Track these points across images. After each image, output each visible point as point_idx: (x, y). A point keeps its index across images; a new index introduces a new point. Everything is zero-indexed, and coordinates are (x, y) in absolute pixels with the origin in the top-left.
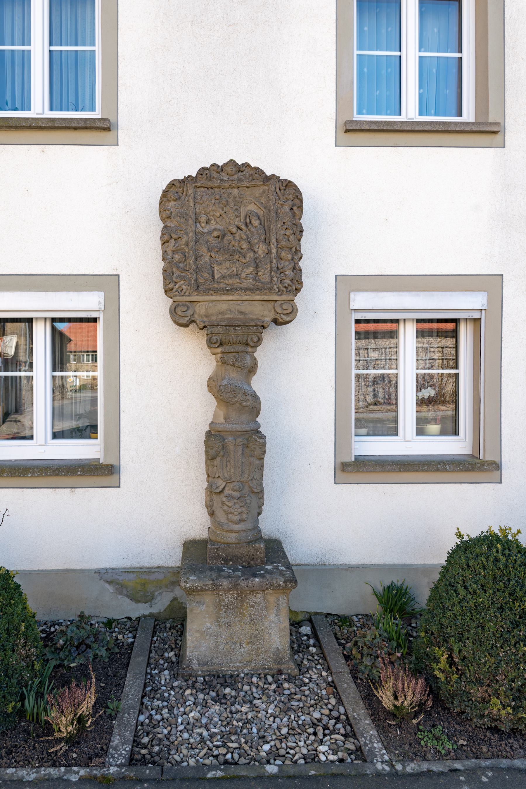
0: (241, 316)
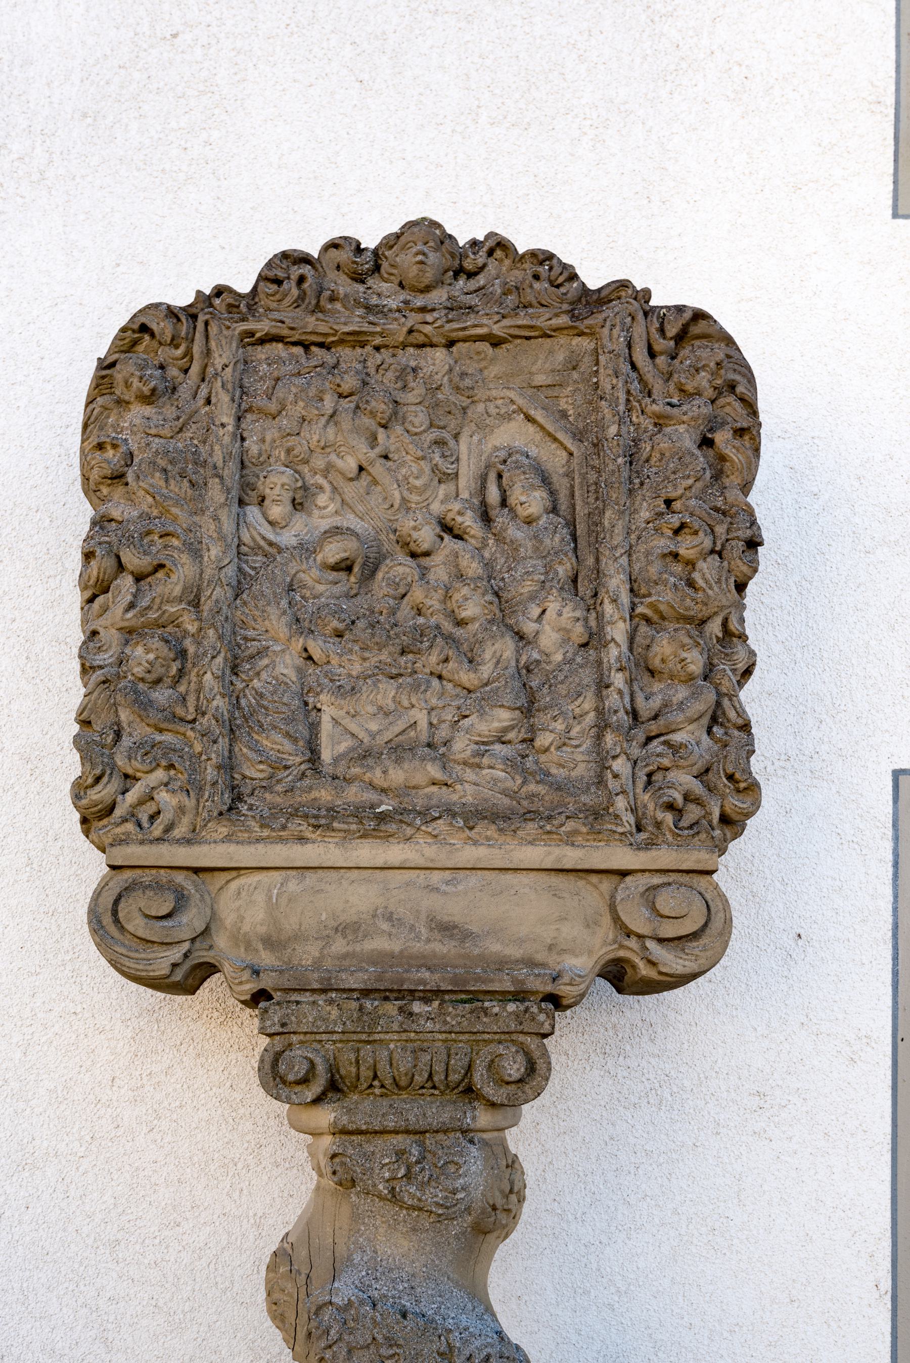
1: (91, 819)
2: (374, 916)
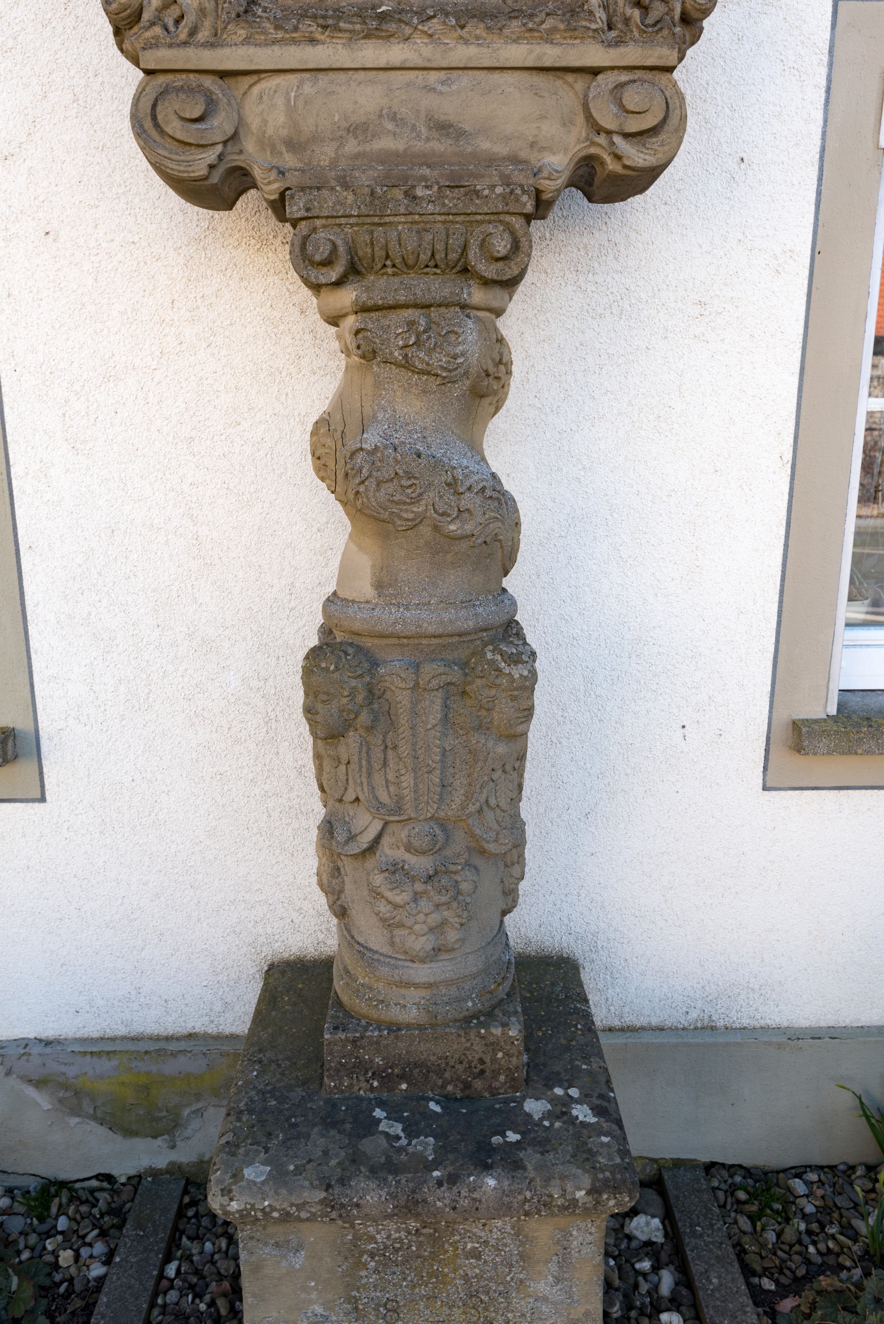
2: (380, 116)
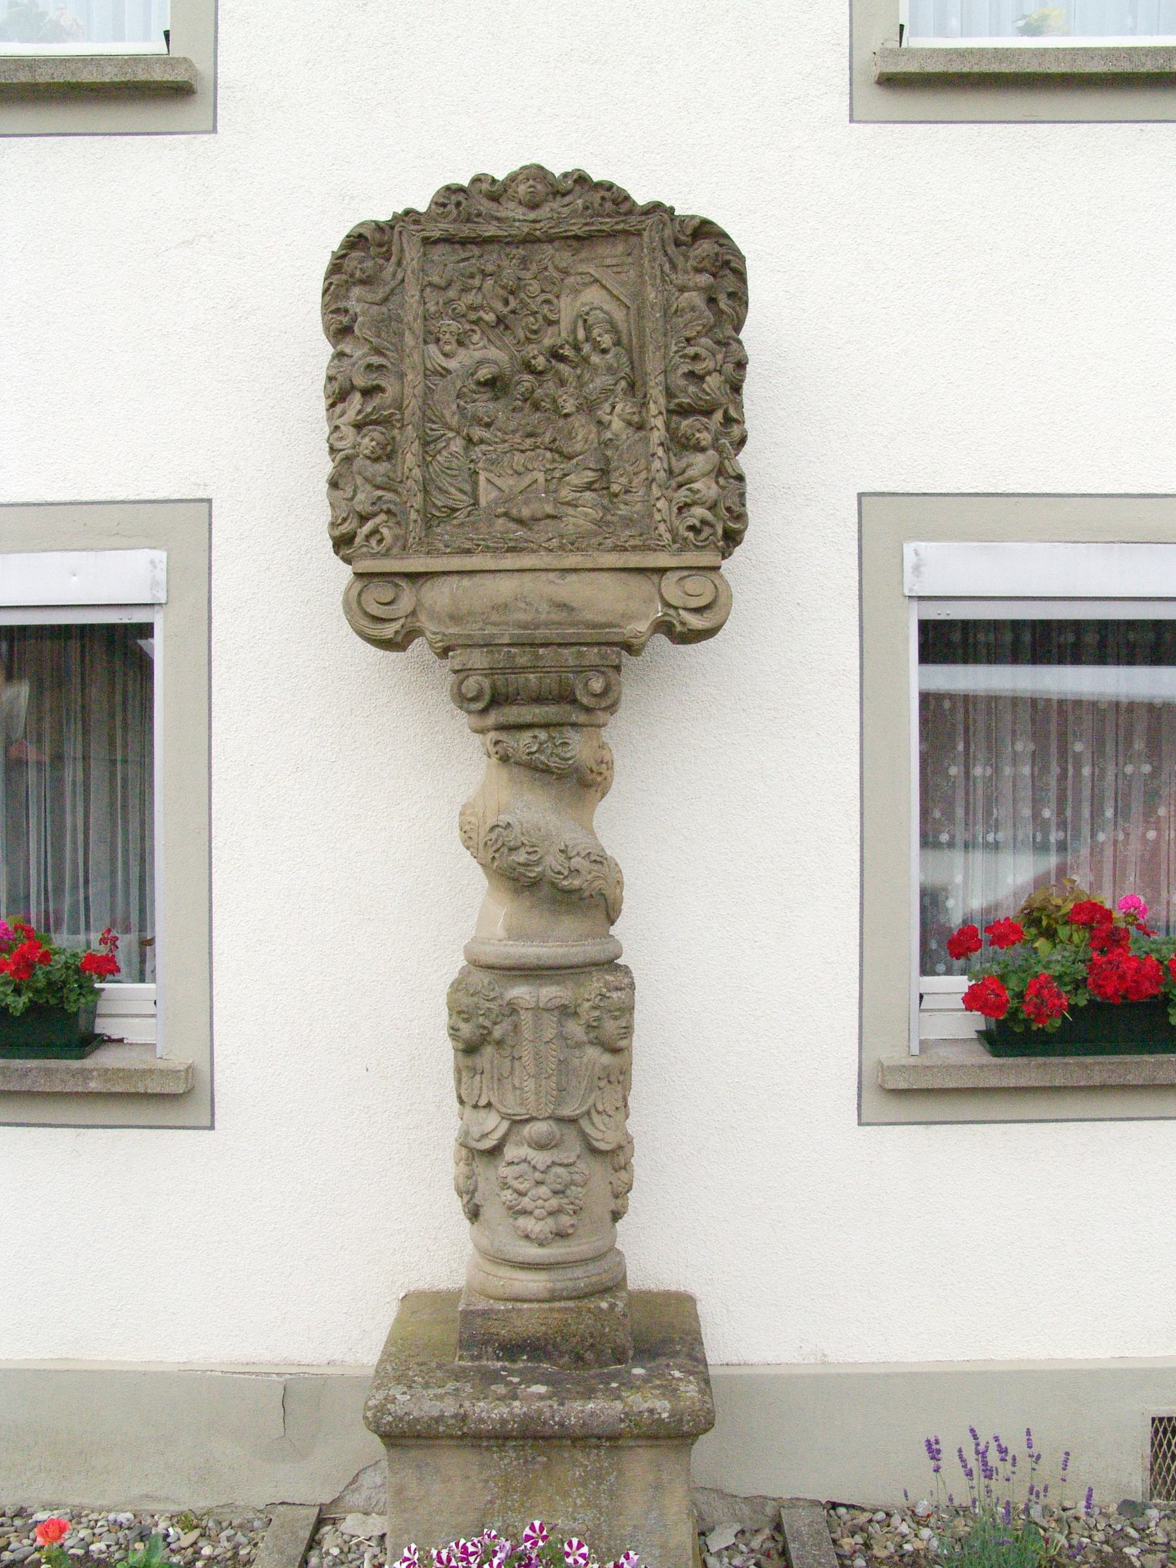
0: (562, 616)
1: (342, 543)
